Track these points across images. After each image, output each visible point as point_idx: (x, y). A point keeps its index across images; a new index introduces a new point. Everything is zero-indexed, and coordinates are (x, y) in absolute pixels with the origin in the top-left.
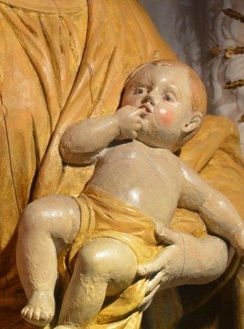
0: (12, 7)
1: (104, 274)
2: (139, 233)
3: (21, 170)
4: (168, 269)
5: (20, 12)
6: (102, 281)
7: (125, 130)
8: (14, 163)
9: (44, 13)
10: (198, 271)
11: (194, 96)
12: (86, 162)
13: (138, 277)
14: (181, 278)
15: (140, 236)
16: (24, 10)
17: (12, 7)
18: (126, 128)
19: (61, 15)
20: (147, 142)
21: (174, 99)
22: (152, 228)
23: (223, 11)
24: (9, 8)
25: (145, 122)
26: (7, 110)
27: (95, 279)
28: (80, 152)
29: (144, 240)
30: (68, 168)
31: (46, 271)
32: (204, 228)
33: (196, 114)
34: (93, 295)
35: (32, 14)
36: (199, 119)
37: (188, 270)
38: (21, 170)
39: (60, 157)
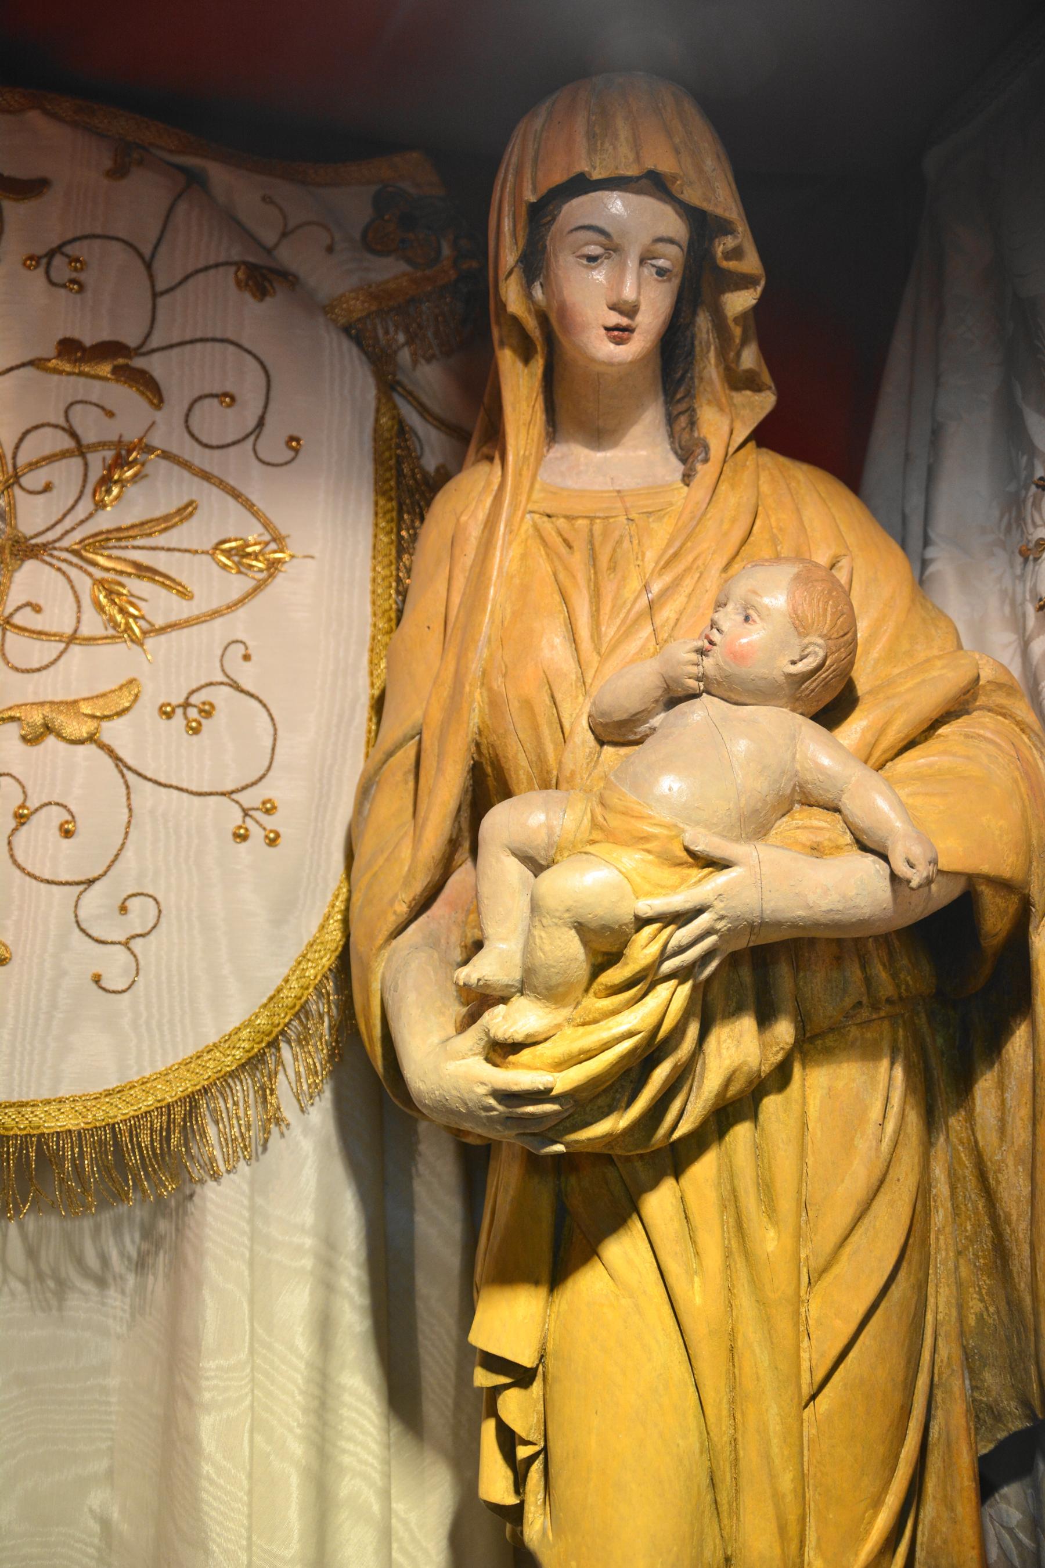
0: (549, 516)
1: (558, 914)
2: (648, 846)
3: (539, 757)
4: (723, 909)
5: (561, 522)
6: (556, 924)
7: (671, 677)
8: (528, 745)
9: (599, 518)
10: (800, 913)
11: (795, 611)
12: (632, 737)
13: (642, 922)
14: (753, 927)
15: (649, 852)
16: (566, 517)
17: (549, 516)
18: (671, 674)
19: (630, 517)
20: (725, 697)
21: (757, 619)
22: (677, 836)
23: (1034, 483)
24: (546, 519)
25: (708, 663)
26: (506, 667)
27: (544, 921)
28: (608, 720)
29: (658, 857)
30: (608, 750)
31: (501, 909)
32: (848, 838)
33: (806, 641)
34: (547, 948)
35: (580, 522)
36: (817, 649)
37: (773, 911)
38: (539, 757)
39: (590, 733)
